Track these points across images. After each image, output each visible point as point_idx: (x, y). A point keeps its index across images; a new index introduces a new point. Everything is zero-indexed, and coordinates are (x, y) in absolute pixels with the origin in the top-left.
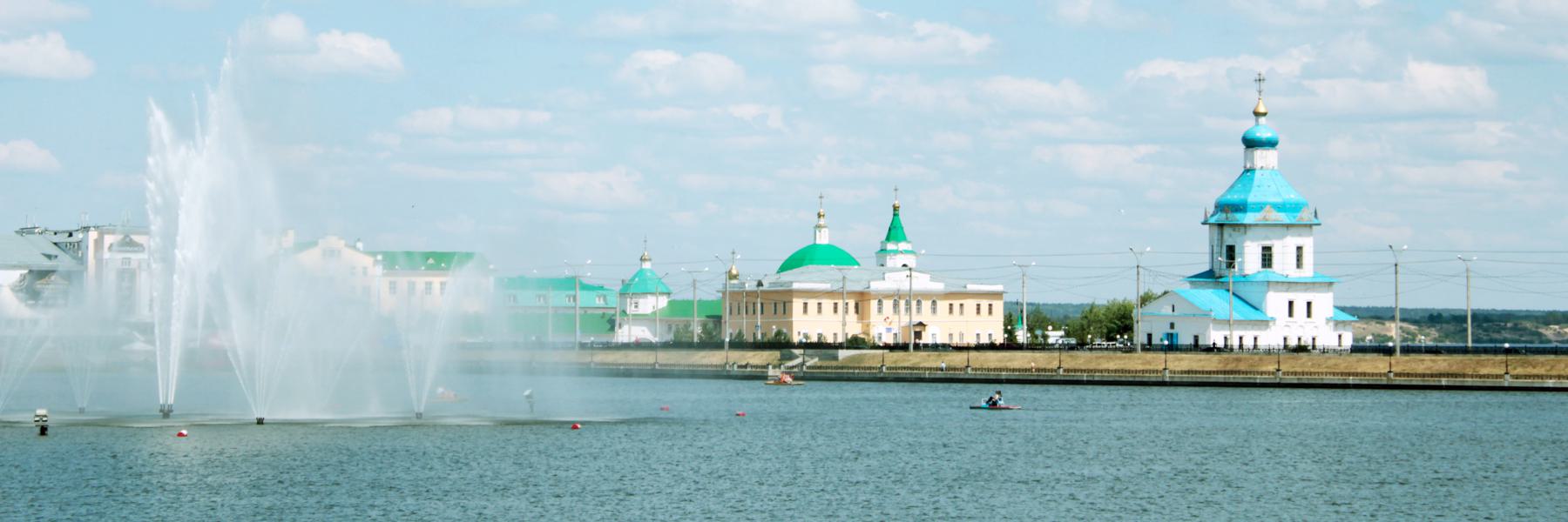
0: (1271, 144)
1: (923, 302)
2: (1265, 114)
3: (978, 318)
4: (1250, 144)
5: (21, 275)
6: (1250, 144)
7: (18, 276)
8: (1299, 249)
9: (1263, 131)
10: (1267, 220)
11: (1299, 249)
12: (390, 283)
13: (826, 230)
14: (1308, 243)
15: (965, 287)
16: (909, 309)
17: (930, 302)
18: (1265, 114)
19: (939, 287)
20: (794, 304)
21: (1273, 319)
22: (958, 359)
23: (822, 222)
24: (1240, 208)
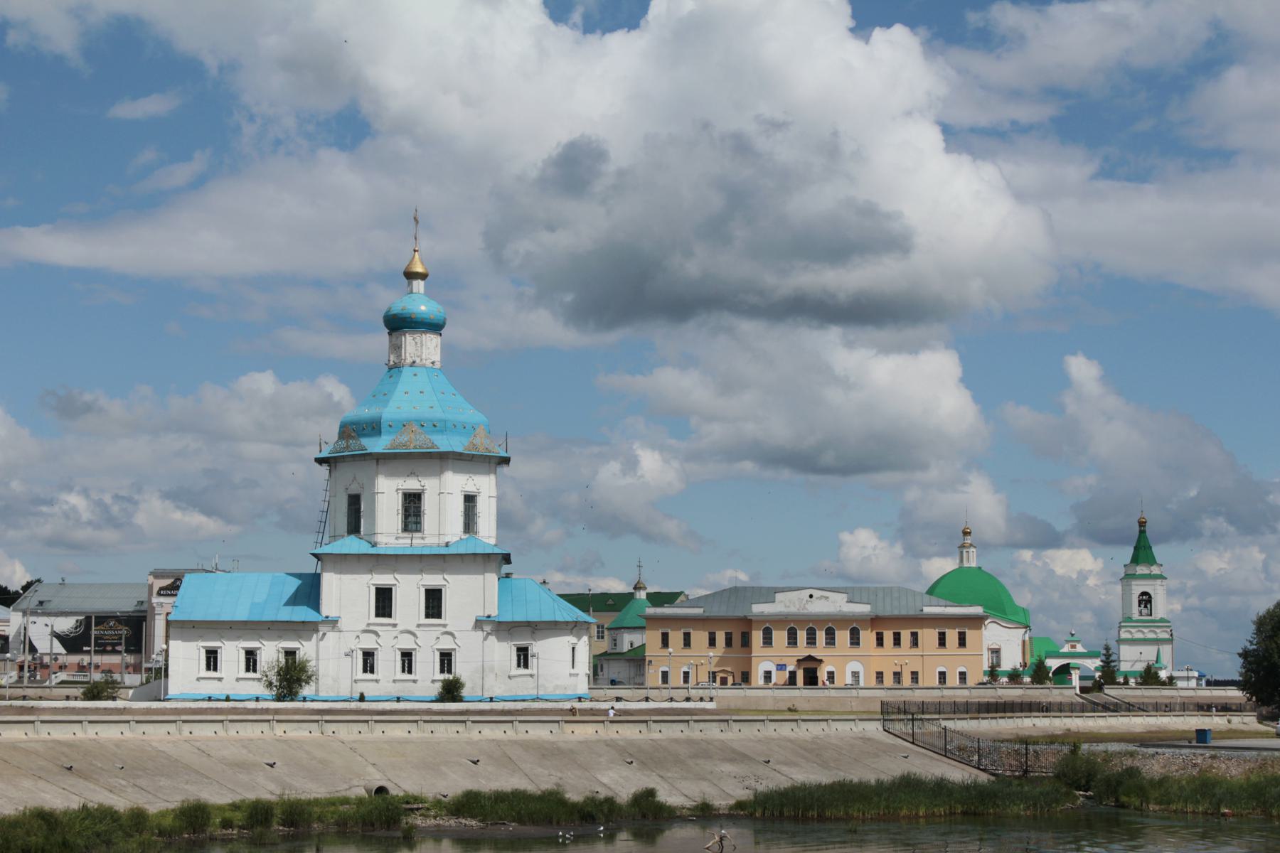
0: (435, 327)
1: (774, 633)
2: (423, 276)
3: (880, 651)
4: (398, 324)
5: (77, 621)
6: (398, 324)
7: (75, 621)
8: (470, 500)
9: (420, 303)
10: (490, 452)
11: (470, 500)
12: (940, 633)
13: (972, 549)
14: (485, 485)
15: (922, 610)
16: (793, 641)
17: (847, 634)
18: (423, 276)
19: (863, 609)
20: (157, 622)
21: (333, 623)
22: (520, 706)
23: (968, 540)
24: (373, 427)
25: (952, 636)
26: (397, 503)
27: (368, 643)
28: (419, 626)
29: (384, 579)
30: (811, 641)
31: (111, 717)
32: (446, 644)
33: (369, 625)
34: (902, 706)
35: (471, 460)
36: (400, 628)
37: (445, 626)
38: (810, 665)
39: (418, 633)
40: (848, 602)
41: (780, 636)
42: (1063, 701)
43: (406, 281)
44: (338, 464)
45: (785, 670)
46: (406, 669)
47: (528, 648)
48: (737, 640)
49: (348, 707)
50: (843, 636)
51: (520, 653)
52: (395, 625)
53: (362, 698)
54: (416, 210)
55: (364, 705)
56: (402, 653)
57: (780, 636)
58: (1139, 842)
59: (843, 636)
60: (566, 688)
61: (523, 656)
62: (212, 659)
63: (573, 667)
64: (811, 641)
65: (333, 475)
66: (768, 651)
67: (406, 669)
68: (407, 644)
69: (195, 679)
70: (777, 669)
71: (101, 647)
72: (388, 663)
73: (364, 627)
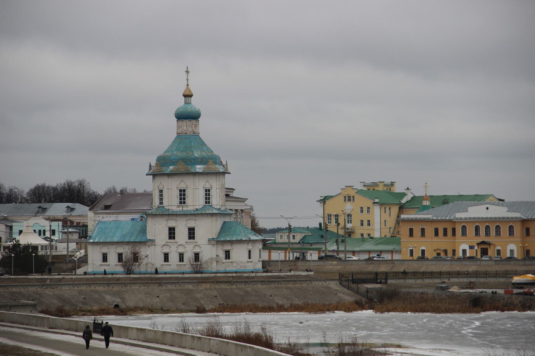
8: (208, 192)
11: (208, 192)
16: (477, 233)
25: (417, 232)
26: (176, 193)
27: (166, 250)
28: (186, 242)
29: (172, 223)
30: (487, 233)
31: (80, 277)
32: (197, 250)
33: (167, 242)
34: (476, 273)
35: (207, 175)
36: (178, 244)
37: (196, 242)
38: (484, 246)
39: (186, 246)
40: (507, 211)
41: (470, 231)
42: (450, 270)
43: (184, 98)
44: (155, 177)
45: (474, 248)
46: (228, 257)
47: (229, 251)
48: (450, 232)
49: (146, 276)
50: (505, 230)
51: (226, 253)
52: (177, 243)
53: (105, 273)
54: (187, 68)
55: (157, 276)
56: (164, 254)
57: (470, 231)
58: (472, 326)
59: (505, 230)
60: (245, 267)
61: (228, 255)
62: (105, 258)
63: (250, 258)
64: (487, 233)
65: (154, 181)
66: (464, 239)
67: (228, 257)
68: (181, 250)
69: (487, 210)
70: (470, 248)
71: (97, 238)
72: (174, 258)
73: (164, 243)
